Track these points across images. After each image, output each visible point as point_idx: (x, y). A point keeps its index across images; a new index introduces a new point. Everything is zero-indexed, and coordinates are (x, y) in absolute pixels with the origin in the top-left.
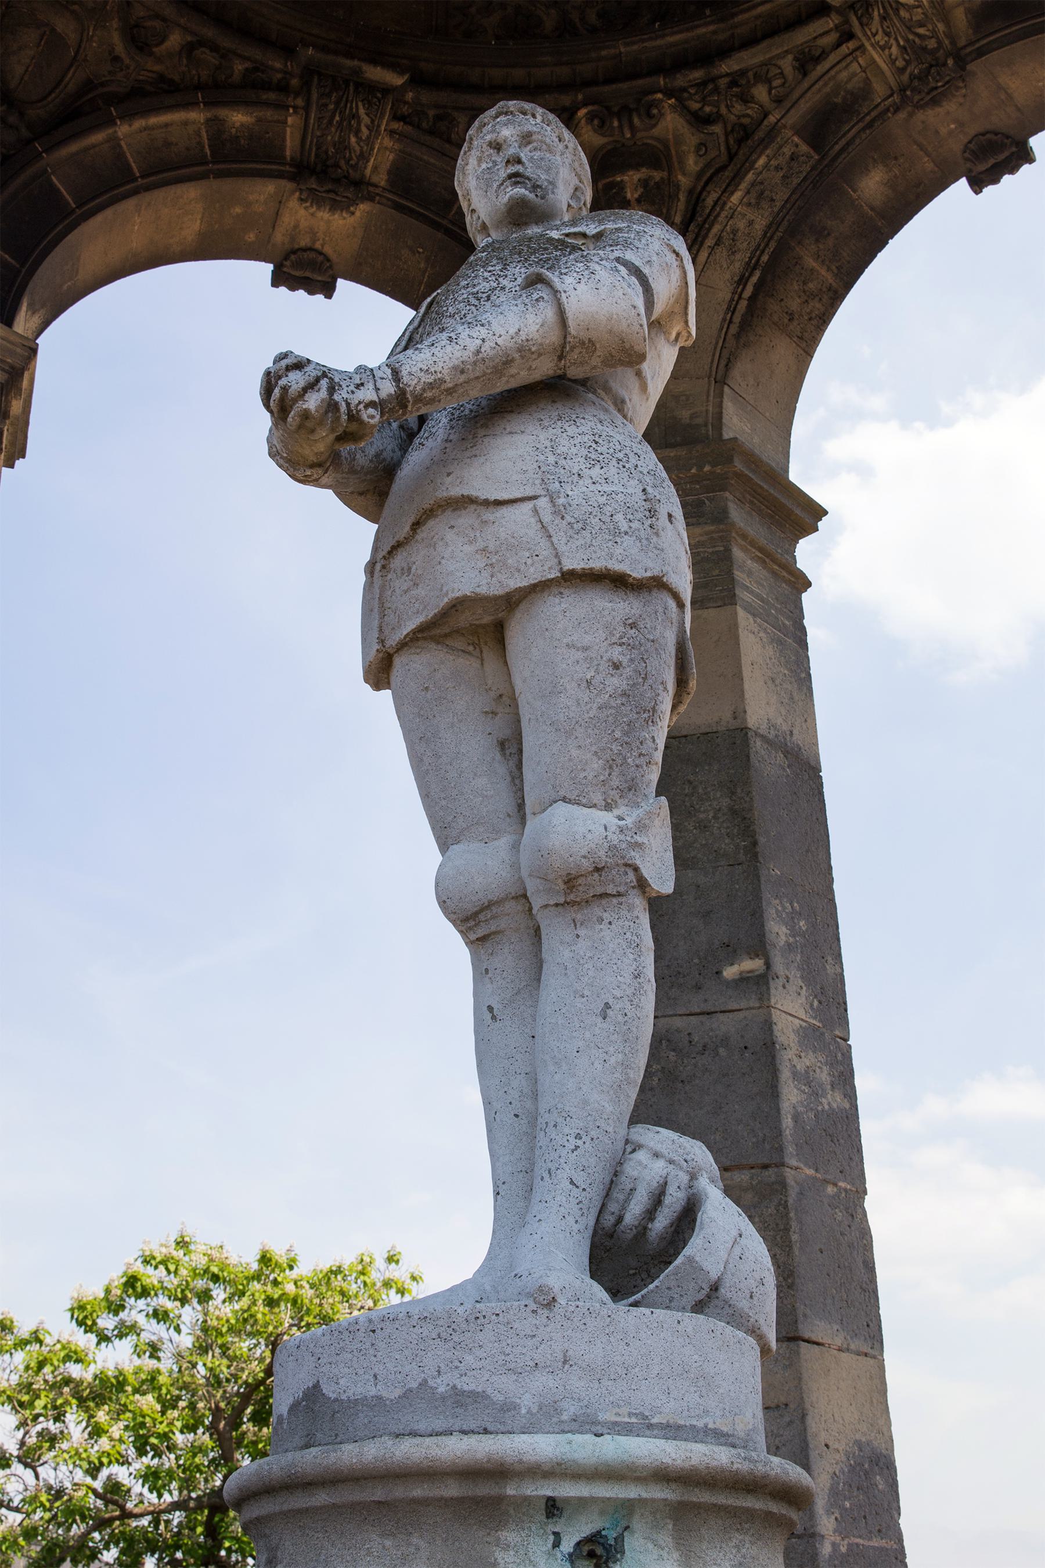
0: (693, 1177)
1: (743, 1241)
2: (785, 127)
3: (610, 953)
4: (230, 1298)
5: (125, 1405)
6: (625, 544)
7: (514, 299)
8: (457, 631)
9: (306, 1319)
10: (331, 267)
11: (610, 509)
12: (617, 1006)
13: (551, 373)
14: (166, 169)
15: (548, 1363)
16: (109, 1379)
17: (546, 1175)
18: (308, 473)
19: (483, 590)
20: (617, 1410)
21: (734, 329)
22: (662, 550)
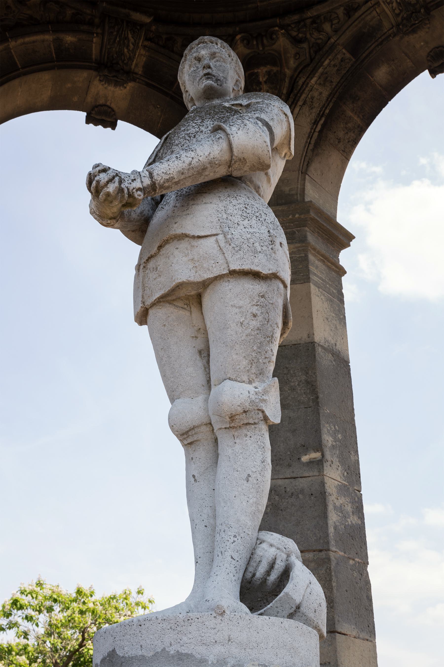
0: (288, 556)
1: (311, 586)
2: (339, 44)
3: (250, 451)
4: (62, 610)
5: (12, 661)
6: (259, 258)
7: (208, 138)
8: (179, 298)
9: (99, 620)
10: (115, 114)
11: (252, 240)
12: (253, 476)
13: (225, 174)
14: (34, 64)
15: (221, 641)
16: (4, 648)
17: (220, 554)
18: (109, 222)
19: (192, 279)
20: (253, 663)
21: (311, 147)
22: (277, 260)
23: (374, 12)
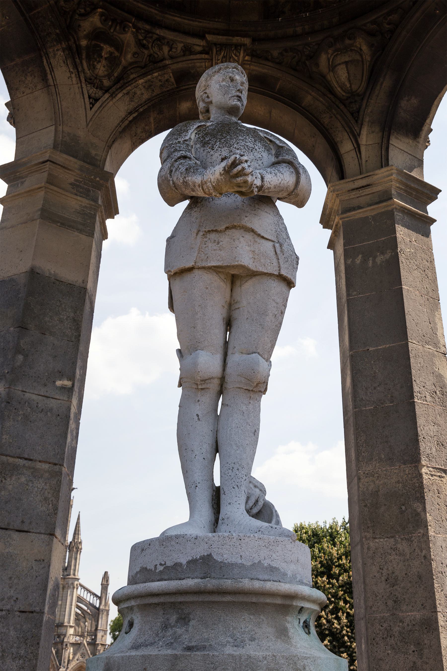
21: (120, 130)
23: (204, 64)
